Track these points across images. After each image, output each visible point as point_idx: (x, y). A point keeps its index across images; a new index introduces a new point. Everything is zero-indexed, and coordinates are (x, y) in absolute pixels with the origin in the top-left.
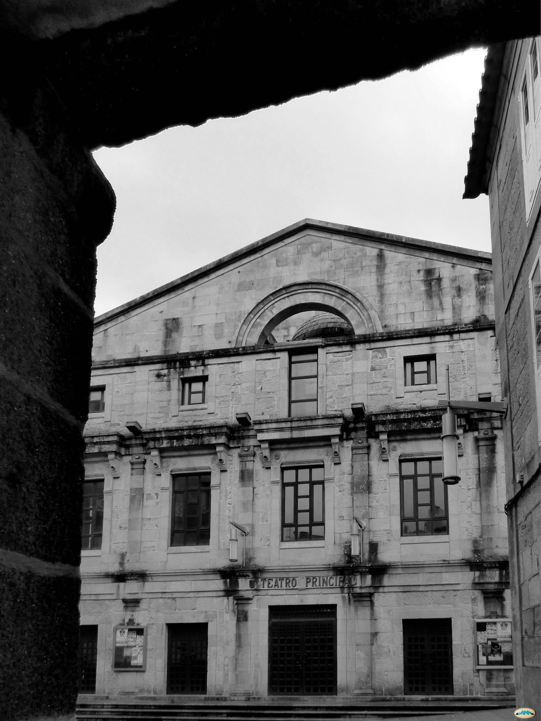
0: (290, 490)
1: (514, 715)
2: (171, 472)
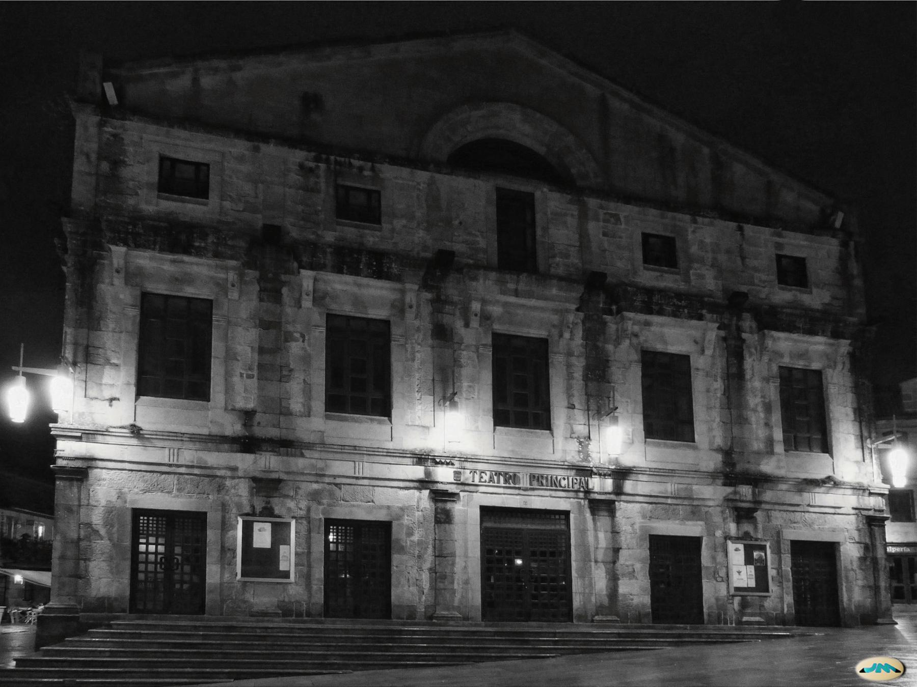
1: (855, 674)
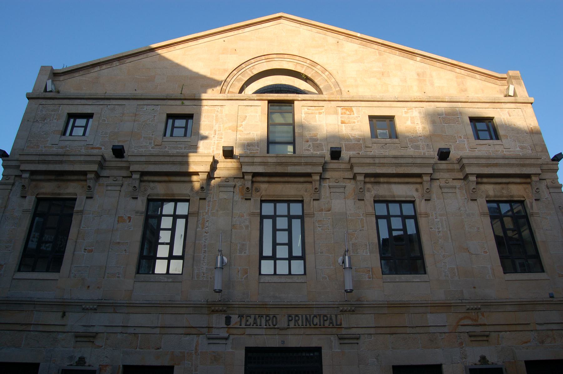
0: (268, 223)
2: (37, 195)
